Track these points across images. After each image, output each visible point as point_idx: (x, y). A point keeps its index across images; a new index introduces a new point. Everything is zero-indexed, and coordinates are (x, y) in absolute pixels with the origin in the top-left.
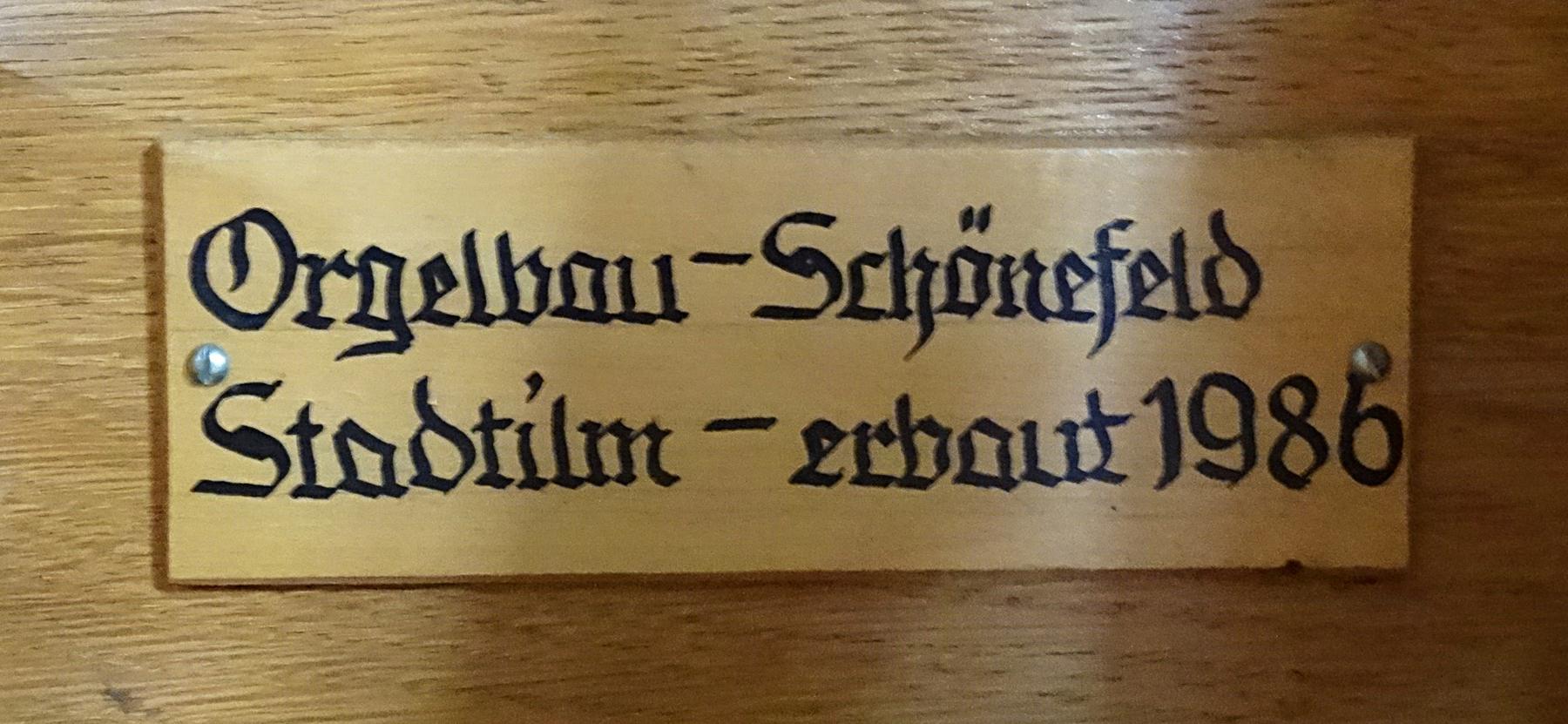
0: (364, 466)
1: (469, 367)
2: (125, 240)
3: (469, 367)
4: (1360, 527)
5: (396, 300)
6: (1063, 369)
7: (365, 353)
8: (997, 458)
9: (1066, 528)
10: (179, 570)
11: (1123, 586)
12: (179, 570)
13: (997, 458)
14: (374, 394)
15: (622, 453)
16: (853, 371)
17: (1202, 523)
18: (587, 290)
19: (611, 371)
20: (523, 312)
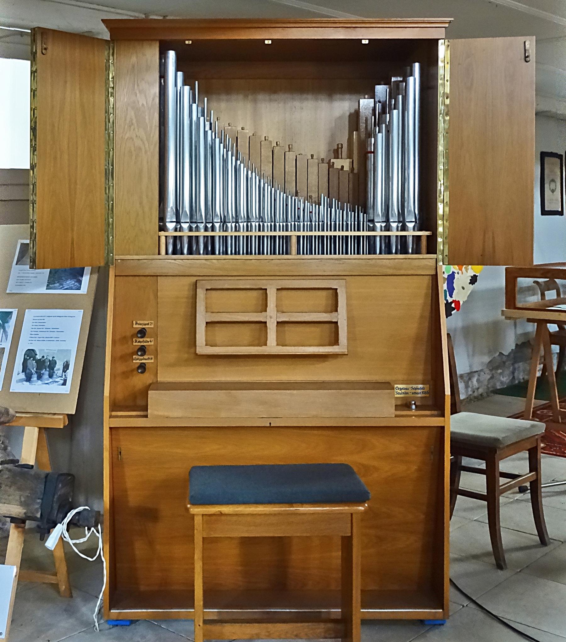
0: (400, 394)
1: (403, 391)
2: (72, 257)
3: (403, 391)
4: (428, 395)
5: (401, 389)
6: (419, 391)
7: (544, 162)
8: (418, 393)
9: (419, 395)
10: (547, 159)
11: (421, 397)
12: (547, 159)
13: (418, 393)
14: (400, 392)
15: (407, 393)
16: (414, 391)
17: (423, 395)
18: (406, 389)
19: (407, 391)
20: (560, 350)
